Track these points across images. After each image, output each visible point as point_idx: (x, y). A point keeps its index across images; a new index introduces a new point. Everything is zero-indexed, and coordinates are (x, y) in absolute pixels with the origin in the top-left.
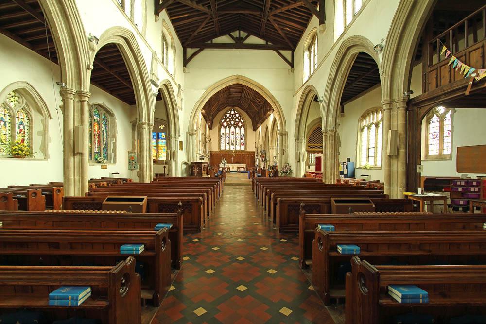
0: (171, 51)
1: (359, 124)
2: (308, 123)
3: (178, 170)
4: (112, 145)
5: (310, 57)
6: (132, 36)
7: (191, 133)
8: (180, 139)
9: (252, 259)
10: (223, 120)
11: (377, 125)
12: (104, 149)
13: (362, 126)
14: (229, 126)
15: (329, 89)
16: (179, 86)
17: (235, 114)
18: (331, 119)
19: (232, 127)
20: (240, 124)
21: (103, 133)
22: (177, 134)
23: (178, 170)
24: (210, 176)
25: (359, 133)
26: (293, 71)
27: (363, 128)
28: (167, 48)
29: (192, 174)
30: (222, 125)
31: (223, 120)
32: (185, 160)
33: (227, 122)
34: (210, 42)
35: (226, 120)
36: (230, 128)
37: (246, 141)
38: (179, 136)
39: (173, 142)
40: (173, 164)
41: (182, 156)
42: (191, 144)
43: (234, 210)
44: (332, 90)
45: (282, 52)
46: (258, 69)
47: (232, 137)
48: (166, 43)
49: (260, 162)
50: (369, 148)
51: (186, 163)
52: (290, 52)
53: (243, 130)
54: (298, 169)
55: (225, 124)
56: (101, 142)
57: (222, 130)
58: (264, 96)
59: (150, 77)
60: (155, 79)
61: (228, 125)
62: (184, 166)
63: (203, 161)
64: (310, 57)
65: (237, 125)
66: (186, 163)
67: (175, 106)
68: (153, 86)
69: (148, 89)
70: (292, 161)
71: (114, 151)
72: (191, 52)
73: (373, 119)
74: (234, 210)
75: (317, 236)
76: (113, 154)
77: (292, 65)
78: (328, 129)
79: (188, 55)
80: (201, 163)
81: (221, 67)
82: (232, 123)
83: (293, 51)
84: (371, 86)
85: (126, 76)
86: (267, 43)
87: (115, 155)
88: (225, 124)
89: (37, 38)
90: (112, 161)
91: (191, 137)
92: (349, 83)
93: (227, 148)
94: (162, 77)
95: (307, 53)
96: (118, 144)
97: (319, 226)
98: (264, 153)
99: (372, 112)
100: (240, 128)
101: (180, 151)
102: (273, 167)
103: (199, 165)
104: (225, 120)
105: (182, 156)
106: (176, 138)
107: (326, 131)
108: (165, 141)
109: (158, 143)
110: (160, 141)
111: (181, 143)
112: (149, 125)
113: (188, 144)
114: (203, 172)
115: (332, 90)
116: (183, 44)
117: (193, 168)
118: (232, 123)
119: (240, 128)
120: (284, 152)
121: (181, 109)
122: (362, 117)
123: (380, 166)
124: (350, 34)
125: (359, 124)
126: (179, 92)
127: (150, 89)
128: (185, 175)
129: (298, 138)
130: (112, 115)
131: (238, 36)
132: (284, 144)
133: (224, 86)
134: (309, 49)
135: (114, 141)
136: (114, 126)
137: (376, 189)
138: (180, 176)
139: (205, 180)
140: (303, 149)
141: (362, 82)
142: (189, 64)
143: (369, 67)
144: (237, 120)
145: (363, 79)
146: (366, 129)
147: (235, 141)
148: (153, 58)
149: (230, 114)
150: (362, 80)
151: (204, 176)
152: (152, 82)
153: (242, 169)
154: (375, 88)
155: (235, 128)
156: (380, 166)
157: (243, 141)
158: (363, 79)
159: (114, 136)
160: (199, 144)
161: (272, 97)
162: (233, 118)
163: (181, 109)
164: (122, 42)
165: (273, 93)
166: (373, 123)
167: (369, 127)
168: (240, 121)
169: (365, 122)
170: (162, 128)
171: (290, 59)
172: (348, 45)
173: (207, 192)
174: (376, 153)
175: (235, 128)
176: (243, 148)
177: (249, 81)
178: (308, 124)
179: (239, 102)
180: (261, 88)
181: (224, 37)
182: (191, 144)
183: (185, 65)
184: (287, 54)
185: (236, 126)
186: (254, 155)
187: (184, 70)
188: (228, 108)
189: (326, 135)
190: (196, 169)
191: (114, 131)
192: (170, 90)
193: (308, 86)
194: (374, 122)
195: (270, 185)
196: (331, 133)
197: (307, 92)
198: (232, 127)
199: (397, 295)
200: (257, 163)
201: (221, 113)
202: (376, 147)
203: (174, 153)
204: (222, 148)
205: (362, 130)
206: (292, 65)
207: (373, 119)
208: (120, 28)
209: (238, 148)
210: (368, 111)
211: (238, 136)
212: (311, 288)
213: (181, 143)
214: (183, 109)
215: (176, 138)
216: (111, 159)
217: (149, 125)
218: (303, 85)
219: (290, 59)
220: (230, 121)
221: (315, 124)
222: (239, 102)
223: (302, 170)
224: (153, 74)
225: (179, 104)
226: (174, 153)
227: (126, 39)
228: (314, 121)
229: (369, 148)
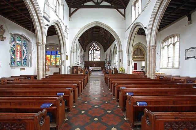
0: (61, 7)
1: (162, 45)
2: (133, 45)
3: (66, 71)
4: (29, 57)
5: (135, 10)
6: (59, 22)
7: (72, 51)
8: (67, 54)
9: (104, 112)
10: (90, 48)
11: (174, 45)
12: (24, 59)
13: (163, 46)
14: (93, 50)
15: (153, 20)
16: (66, 27)
17: (96, 45)
18: (153, 39)
19: (95, 51)
20: (98, 49)
21: (24, 51)
22: (65, 52)
23: (66, 71)
24: (82, 74)
25: (161, 50)
26: (125, 19)
27: (164, 47)
28: (59, 5)
29: (73, 72)
30: (90, 50)
31: (90, 48)
32: (70, 65)
33: (92, 48)
34: (83, 5)
35: (92, 48)
36: (93, 51)
37: (101, 57)
38: (66, 53)
39: (63, 56)
40: (63, 67)
41: (68, 64)
42: (73, 57)
43: (95, 87)
44: (154, 21)
45: (119, 9)
46: (108, 19)
47: (95, 55)
48: (59, 2)
49: (107, 66)
50: (168, 58)
51: (70, 67)
52: (123, 10)
53: (99, 52)
54: (128, 69)
55: (91, 49)
56: (22, 56)
57: (90, 52)
58: (110, 32)
59: (43, 14)
60: (47, 16)
61: (93, 50)
62: (69, 68)
63: (78, 66)
64: (135, 10)
65: (97, 50)
66: (70, 67)
67: (63, 37)
68: (44, 20)
69: (41, 22)
70: (125, 66)
71: (31, 61)
72: (72, 10)
73: (171, 42)
74: (95, 87)
75: (128, 98)
76: (30, 62)
77: (124, 16)
78: (151, 45)
79: (71, 12)
80: (78, 67)
81: (86, 19)
82: (95, 49)
83: (125, 9)
84: (171, 23)
85: (27, 13)
86: (111, 5)
87: (31, 63)
88: (91, 49)
89: (26, 20)
90: (29, 66)
91: (72, 53)
92: (167, 14)
93: (92, 60)
94: (53, 19)
95: (133, 8)
96: (33, 57)
97: (127, 93)
98: (109, 62)
99: (170, 38)
100: (98, 51)
101: (67, 61)
102: (114, 69)
103: (76, 67)
104: (92, 48)
105: (68, 64)
106: (64, 54)
107: (150, 47)
108: (59, 55)
109: (56, 57)
110: (57, 55)
111: (67, 56)
112: (43, 44)
113: (70, 58)
114: (78, 71)
115: (154, 21)
116: (68, 5)
117: (74, 69)
118: (95, 49)
119: (98, 51)
120: (120, 60)
121: (67, 39)
122: (163, 41)
123: (178, 67)
124: (136, 21)
125: (162, 45)
126: (66, 30)
127: (43, 21)
128: (69, 73)
129: (128, 53)
130: (29, 41)
131: (97, 2)
132: (121, 56)
133: (89, 27)
134: (135, 5)
135: (31, 55)
136: (31, 47)
137: (170, 80)
138: (66, 73)
139: (79, 77)
140: (131, 59)
141: (168, 20)
142: (72, 16)
143: (176, 7)
144: (97, 47)
145: (168, 17)
146: (166, 47)
147: (96, 57)
148: (45, 3)
149: (94, 44)
150: (171, 17)
151: (79, 74)
152: (44, 17)
153: (99, 70)
154: (172, 24)
155: (96, 51)
156: (178, 67)
157: (100, 57)
158: (168, 17)
159: (31, 53)
160: (78, 57)
161: (114, 32)
162: (95, 46)
163: (67, 39)
164: (54, 24)
165: (115, 30)
166: (171, 44)
167: (168, 46)
168: (98, 48)
169: (164, 44)
170: (58, 49)
171: (123, 13)
172: (137, 24)
173: (81, 81)
174: (173, 60)
175: (96, 51)
176: (99, 60)
177: (103, 24)
178: (133, 45)
179: (97, 37)
180: (109, 28)
181: (90, 2)
182: (73, 57)
183: (70, 16)
184: (122, 10)
185: (96, 50)
186: (104, 63)
187: (69, 19)
188: (93, 42)
189: (150, 49)
190: (75, 70)
191: (31, 50)
192: (60, 27)
193: (135, 24)
194: (172, 43)
195: (113, 78)
196: (153, 47)
197: (134, 27)
198: (95, 51)
199: (138, 104)
200: (106, 67)
201: (89, 44)
202: (173, 57)
203: (63, 61)
204: (90, 60)
205: (163, 48)
206: (124, 16)
207: (171, 42)
208: (55, 20)
209: (97, 60)
210: (172, 35)
211: (97, 54)
212: (125, 119)
213: (67, 56)
214: (68, 39)
215: (64, 54)
216: (29, 65)
217: (43, 44)
218: (132, 24)
219: (123, 13)
220: (93, 48)
221: (137, 46)
222: (97, 37)
223: (130, 71)
224: (45, 13)
225: (66, 34)
226: (63, 61)
227: (57, 24)
228: (136, 44)
229: (168, 58)
